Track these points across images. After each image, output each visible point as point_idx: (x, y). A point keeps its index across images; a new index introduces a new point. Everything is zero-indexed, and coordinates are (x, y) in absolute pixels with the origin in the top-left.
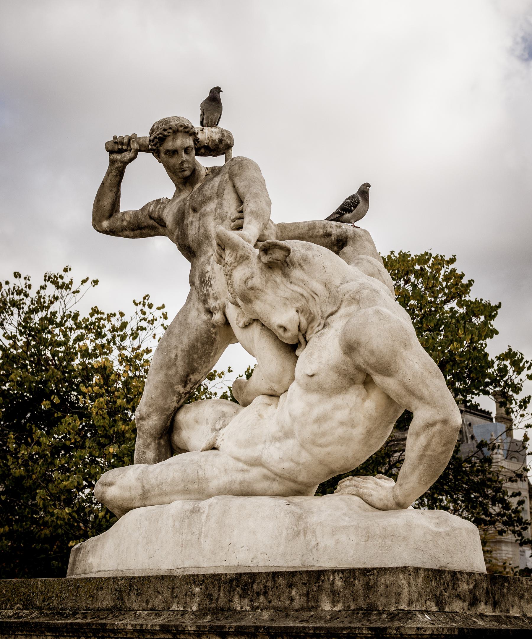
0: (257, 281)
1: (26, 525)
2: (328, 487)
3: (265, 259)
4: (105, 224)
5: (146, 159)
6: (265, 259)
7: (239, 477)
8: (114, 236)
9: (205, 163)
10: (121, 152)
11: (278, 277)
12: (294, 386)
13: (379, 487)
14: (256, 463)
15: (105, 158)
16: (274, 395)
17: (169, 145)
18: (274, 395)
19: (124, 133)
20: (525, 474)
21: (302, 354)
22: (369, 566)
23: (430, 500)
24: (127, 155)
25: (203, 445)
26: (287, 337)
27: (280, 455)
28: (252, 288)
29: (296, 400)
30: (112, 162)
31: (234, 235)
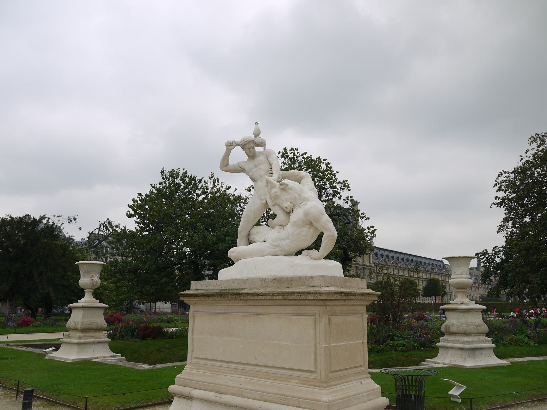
0: (278, 194)
1: (530, 315)
2: (299, 253)
3: (281, 187)
4: (225, 168)
5: (238, 148)
6: (281, 187)
7: (272, 250)
8: (331, 277)
9: (258, 149)
10: (230, 146)
11: (284, 193)
12: (289, 225)
13: (314, 252)
14: (278, 246)
15: (225, 147)
16: (283, 226)
17: (247, 146)
18: (283, 226)
19: (231, 139)
20: (355, 208)
21: (292, 215)
22: (313, 275)
23: (327, 257)
24: (232, 147)
25: (262, 240)
26: (288, 210)
27: (286, 244)
28: (277, 196)
29: (289, 228)
30: (227, 149)
31: (270, 179)
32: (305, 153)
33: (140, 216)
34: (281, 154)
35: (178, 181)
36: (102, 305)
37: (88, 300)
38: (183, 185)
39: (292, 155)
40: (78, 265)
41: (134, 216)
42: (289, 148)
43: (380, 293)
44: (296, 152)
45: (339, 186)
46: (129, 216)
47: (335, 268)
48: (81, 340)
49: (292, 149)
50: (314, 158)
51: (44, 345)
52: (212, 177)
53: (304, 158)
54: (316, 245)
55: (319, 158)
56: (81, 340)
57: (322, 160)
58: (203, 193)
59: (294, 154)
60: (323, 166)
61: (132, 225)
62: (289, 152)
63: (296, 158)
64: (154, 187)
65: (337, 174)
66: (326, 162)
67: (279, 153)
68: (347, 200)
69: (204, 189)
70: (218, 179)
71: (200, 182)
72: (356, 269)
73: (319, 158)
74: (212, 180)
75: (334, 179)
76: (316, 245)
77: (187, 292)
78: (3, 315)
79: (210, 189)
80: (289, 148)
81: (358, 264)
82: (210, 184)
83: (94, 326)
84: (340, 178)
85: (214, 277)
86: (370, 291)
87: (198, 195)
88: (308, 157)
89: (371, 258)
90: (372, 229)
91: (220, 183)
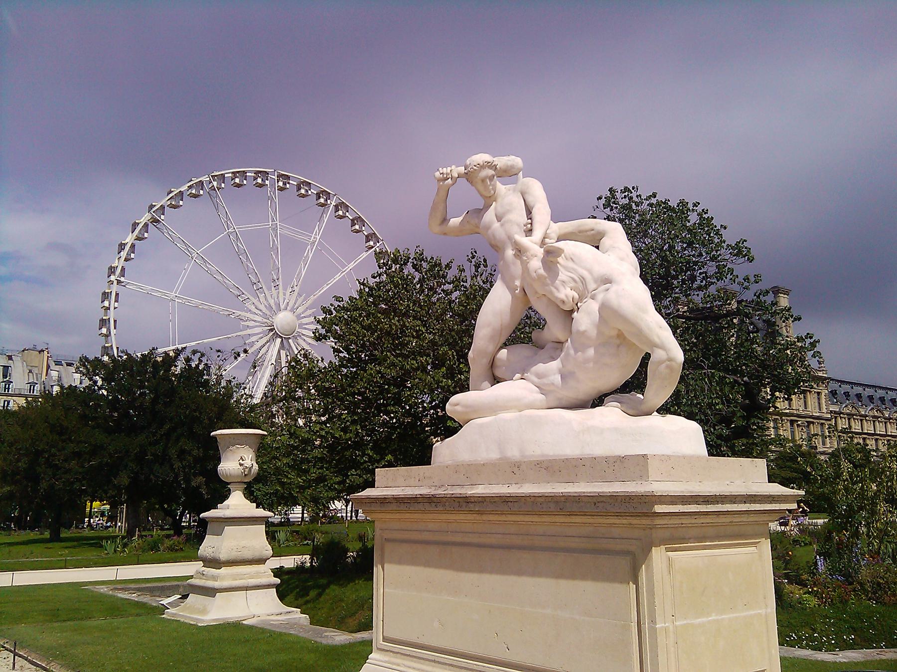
2: (598, 401)
23: (664, 410)
32: (654, 195)
33: (338, 338)
34: (603, 201)
35: (409, 269)
36: (262, 512)
37: (237, 503)
38: (418, 276)
39: (626, 201)
40: (215, 437)
41: (325, 337)
42: (619, 187)
43: (802, 493)
44: (634, 195)
45: (724, 253)
46: (319, 338)
47: (685, 435)
48: (236, 579)
49: (626, 189)
50: (673, 203)
51: (164, 587)
52: (473, 257)
53: (651, 205)
54: (637, 383)
55: (683, 203)
56: (236, 579)
57: (690, 206)
58: (456, 288)
59: (631, 198)
60: (693, 218)
61: (325, 354)
62: (618, 195)
63: (634, 207)
64: (363, 284)
65: (722, 231)
66: (699, 209)
67: (599, 198)
68: (746, 284)
69: (457, 283)
70: (485, 260)
71: (448, 266)
72: (792, 425)
73: (683, 203)
74: (473, 263)
75: (716, 240)
76: (637, 383)
77: (368, 492)
78: (895, 412)
79: (469, 280)
80: (619, 187)
81: (811, 417)
82: (469, 270)
83: (248, 555)
84: (730, 237)
85: (423, 457)
86: (777, 489)
87: (448, 293)
88: (659, 204)
89: (823, 401)
90: (808, 341)
91: (489, 269)
